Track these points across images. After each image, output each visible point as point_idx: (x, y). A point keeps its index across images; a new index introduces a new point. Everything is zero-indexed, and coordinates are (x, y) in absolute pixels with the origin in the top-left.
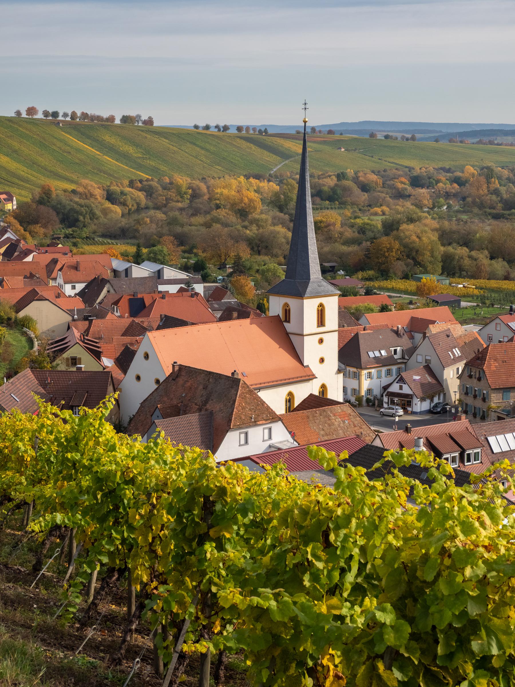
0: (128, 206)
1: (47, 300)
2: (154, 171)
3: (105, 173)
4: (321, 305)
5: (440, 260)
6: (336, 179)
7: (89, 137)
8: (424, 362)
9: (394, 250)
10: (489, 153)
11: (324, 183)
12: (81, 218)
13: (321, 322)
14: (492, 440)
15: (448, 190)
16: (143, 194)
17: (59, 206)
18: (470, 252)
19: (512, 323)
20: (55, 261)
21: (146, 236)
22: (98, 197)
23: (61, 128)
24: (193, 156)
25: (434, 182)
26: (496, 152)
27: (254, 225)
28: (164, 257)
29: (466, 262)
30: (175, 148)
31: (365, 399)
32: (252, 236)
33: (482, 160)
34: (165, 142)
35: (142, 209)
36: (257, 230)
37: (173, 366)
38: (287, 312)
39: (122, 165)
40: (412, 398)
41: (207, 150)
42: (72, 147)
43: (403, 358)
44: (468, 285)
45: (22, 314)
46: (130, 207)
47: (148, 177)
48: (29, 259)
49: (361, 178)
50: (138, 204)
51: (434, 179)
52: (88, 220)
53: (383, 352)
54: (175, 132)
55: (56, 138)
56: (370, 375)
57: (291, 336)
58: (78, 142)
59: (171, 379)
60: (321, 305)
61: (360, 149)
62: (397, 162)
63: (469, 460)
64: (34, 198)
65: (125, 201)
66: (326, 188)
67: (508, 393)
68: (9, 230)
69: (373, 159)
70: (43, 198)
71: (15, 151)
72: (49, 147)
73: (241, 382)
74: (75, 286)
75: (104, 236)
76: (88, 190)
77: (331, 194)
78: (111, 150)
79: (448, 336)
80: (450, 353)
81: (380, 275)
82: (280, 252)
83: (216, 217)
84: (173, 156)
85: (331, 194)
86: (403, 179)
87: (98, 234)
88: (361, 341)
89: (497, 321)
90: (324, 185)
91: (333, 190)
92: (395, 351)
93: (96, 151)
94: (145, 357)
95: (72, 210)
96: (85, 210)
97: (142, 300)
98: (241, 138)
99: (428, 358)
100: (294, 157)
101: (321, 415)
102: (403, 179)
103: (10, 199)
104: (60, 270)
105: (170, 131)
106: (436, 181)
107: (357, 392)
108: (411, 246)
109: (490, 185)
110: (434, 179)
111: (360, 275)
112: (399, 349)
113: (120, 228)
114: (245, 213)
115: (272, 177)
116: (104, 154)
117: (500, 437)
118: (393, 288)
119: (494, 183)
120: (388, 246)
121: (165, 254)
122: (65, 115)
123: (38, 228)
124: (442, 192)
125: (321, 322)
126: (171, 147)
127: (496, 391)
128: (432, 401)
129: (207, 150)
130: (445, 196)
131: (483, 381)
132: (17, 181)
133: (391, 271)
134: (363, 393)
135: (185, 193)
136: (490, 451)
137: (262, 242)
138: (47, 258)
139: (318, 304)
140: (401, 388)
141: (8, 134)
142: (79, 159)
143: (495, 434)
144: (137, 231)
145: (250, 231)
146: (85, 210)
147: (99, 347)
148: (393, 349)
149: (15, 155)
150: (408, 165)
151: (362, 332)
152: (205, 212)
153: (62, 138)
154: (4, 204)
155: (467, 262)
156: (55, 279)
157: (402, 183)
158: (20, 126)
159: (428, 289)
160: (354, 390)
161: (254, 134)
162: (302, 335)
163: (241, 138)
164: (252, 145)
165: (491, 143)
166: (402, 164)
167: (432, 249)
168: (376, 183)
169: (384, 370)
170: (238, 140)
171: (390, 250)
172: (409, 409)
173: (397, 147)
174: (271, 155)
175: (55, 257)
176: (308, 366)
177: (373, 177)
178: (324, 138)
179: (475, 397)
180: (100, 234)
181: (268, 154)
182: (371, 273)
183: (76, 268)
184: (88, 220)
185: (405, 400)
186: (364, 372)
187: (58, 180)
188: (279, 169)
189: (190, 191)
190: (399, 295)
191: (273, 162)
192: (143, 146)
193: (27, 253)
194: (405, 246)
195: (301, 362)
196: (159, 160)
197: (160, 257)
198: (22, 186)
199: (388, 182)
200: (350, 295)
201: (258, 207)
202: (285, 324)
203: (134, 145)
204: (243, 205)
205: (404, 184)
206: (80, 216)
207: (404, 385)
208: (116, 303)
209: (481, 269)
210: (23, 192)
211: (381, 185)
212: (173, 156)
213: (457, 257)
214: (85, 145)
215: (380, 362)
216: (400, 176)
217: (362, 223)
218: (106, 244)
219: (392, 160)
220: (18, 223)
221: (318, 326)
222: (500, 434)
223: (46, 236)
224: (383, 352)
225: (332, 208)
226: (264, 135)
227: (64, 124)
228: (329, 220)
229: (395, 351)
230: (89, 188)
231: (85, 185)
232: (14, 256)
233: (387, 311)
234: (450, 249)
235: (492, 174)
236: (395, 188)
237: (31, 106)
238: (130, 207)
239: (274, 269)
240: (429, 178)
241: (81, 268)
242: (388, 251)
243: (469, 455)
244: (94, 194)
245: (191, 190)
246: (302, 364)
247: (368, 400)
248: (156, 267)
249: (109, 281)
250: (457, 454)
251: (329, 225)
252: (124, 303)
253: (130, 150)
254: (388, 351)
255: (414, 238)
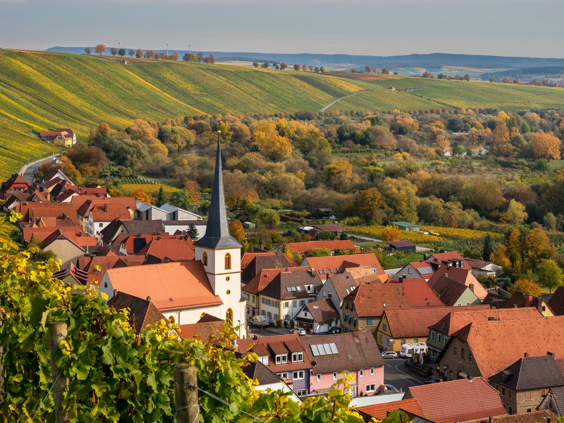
0: (178, 144)
1: (66, 239)
2: (211, 108)
3: (163, 109)
4: (228, 254)
5: (416, 209)
6: (370, 123)
7: (151, 75)
8: (327, 296)
9: (377, 200)
10: (538, 95)
11: (358, 127)
12: (129, 157)
13: (228, 265)
14: (313, 347)
15: (480, 134)
16: (193, 132)
17: (111, 145)
18: (445, 202)
19: (421, 268)
20: (88, 203)
21: (180, 176)
22: (150, 135)
23: (125, 66)
24: (249, 94)
25: (469, 125)
26: (545, 94)
27: (270, 172)
28: (185, 199)
29: (440, 211)
30: (231, 86)
31: (283, 322)
32: (266, 182)
33: (528, 102)
34: (223, 80)
35: (192, 146)
36: (272, 176)
37: (114, 292)
38: (205, 258)
39: (180, 102)
40: (313, 322)
41: (262, 88)
42: (134, 84)
43: (315, 293)
44: (434, 232)
45: (46, 249)
46: (180, 144)
47: (203, 113)
48: (68, 200)
49: (398, 121)
50: (188, 142)
51: (469, 123)
52: (135, 159)
53: (299, 288)
54: (233, 70)
55: (120, 76)
56: (287, 305)
57: (208, 275)
58: (141, 79)
59: (112, 300)
60: (228, 254)
61: (410, 89)
62: (446, 103)
63: (295, 359)
64: (92, 135)
65: (176, 139)
66: (359, 132)
67: (371, 321)
68: (59, 170)
69: (422, 99)
70: (99, 136)
71: (81, 89)
72: (113, 84)
73: (150, 303)
74: (102, 224)
75: (147, 174)
76: (142, 128)
77: (364, 137)
78: (170, 87)
79: (348, 277)
80: (347, 290)
81: (364, 221)
82: (290, 197)
83: (247, 159)
84: (229, 93)
85: (364, 137)
86: (439, 123)
87: (143, 172)
88: (282, 280)
89: (409, 266)
90: (358, 129)
91: (366, 134)
92: (309, 288)
93: (156, 88)
94: (107, 285)
95: (122, 149)
96: (133, 150)
97: (144, 240)
98: (296, 76)
99: (330, 293)
100: (346, 95)
101: (205, 327)
102: (439, 123)
103: (70, 135)
104: (91, 210)
105: (229, 69)
106: (471, 125)
107: (278, 317)
108: (393, 196)
109: (512, 133)
110: (469, 123)
111: (347, 220)
112: (311, 286)
113: (161, 168)
114: (277, 155)
115: (322, 115)
116: (164, 91)
117: (320, 346)
118: (369, 233)
119: (516, 131)
120: (372, 196)
121: (186, 197)
122: (131, 52)
123: (88, 167)
124: (475, 136)
125: (228, 265)
126: (228, 85)
127: (361, 319)
128: (330, 324)
129: (262, 88)
130: (478, 139)
131: (354, 312)
132: (79, 117)
133: (373, 218)
134: (282, 318)
135: (227, 134)
136: (311, 354)
137: (276, 187)
138: (85, 198)
139: (225, 254)
140: (306, 315)
141: (76, 72)
142: (140, 96)
143: (316, 343)
144: (174, 171)
145: (265, 176)
146: (133, 150)
147: (86, 278)
148: (307, 286)
149: (81, 92)
150: (456, 106)
151: (283, 273)
152: (240, 154)
153: (126, 75)
154: (65, 140)
155: (442, 211)
156: (87, 217)
157: (437, 126)
158: (88, 64)
159: (391, 236)
160: (276, 315)
161: (311, 72)
162: (214, 274)
163: (296, 76)
164: (306, 83)
165: (545, 83)
166: (451, 104)
167: (408, 200)
168: (413, 126)
169: (298, 301)
170: (293, 78)
171: (373, 199)
172: (312, 331)
173: (446, 87)
174: (324, 93)
175: (89, 199)
176: (218, 296)
177: (410, 120)
178: (377, 77)
179: (350, 322)
180: (145, 172)
181: (321, 92)
182: (356, 219)
183: (103, 209)
184: (135, 159)
185: (308, 324)
186: (283, 303)
187: (119, 116)
188: (330, 108)
189: (232, 133)
190: (371, 239)
191: (325, 100)
192: (202, 84)
193: (69, 193)
194: (387, 196)
195: (213, 292)
196: (215, 97)
197: (181, 199)
198: (84, 121)
199: (424, 126)
200: (327, 239)
201: (288, 150)
202: (204, 266)
203: (193, 83)
204: (275, 148)
205: (440, 127)
206: (128, 155)
207: (307, 313)
208: (124, 242)
209: (452, 218)
210: (85, 128)
211: (418, 128)
212: (229, 93)
213: (433, 207)
214: (147, 83)
215: (297, 295)
216: (437, 119)
217: (373, 170)
218: (145, 183)
219: (440, 100)
220: (71, 162)
221: (226, 269)
222: (320, 343)
223: (94, 174)
224: (299, 288)
225: (361, 152)
226: (321, 74)
227: (129, 62)
228: (341, 167)
229: (309, 288)
230: (143, 126)
231: (139, 123)
232: (59, 195)
233: (338, 255)
234: (427, 200)
235: (513, 123)
236: (431, 131)
237: (100, 44)
238: (180, 144)
239: (270, 214)
240: (465, 122)
241: (108, 209)
242: (371, 201)
243: (295, 356)
244: (147, 132)
245: (232, 132)
246: (214, 294)
247: (286, 324)
248: (173, 209)
249: (123, 223)
250: (286, 355)
251: (340, 172)
252: (130, 242)
253: (189, 87)
254: (302, 287)
255: (395, 190)
